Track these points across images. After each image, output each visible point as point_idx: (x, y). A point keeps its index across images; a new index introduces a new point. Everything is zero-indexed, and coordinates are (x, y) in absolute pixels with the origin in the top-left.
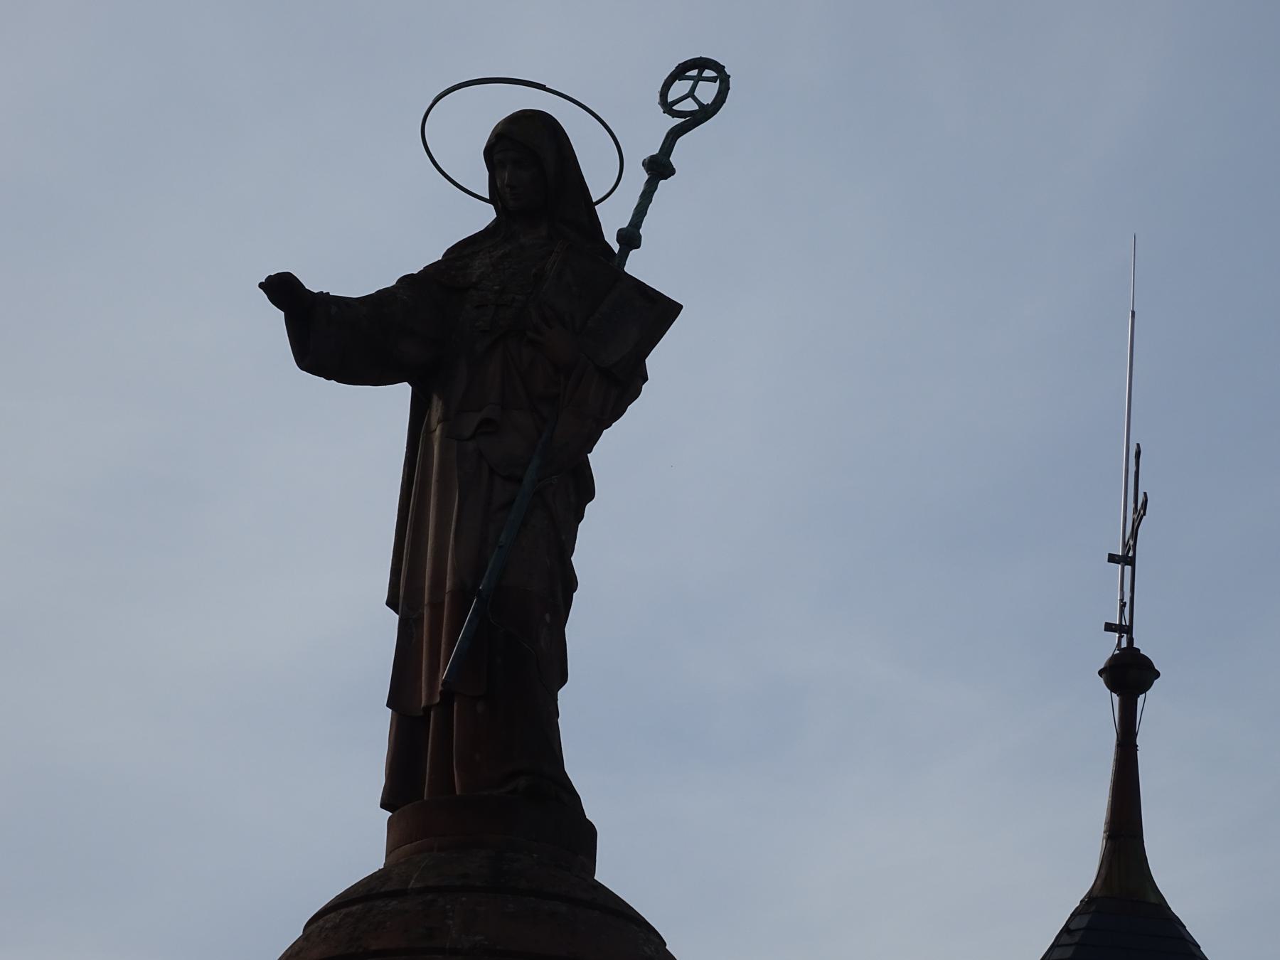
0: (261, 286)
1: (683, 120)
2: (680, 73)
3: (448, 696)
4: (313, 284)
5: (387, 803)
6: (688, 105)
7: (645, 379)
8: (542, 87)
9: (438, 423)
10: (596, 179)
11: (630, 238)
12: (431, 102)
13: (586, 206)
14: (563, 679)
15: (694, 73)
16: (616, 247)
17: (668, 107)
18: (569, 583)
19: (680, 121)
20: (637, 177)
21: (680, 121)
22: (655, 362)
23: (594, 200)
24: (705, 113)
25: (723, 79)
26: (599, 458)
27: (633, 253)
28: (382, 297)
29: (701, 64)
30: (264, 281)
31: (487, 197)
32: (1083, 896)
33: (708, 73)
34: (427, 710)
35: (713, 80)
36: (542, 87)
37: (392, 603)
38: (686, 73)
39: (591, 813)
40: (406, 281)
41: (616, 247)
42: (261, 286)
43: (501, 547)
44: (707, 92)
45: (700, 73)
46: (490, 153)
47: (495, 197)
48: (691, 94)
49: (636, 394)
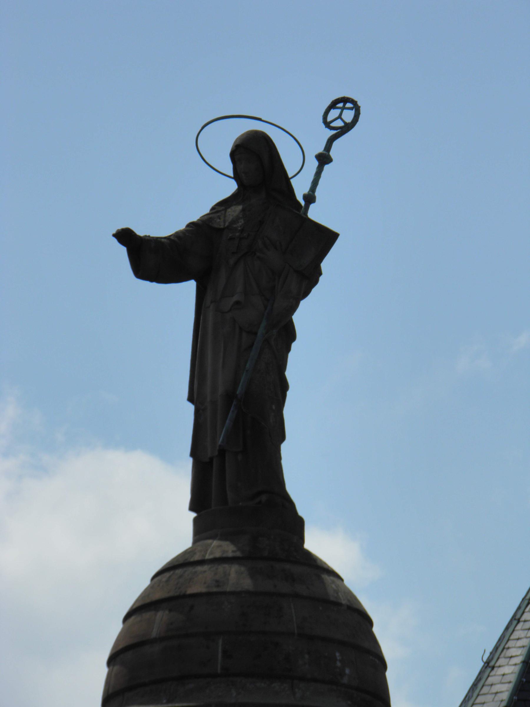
0: (114, 235)
1: (338, 131)
2: (333, 105)
3: (222, 452)
4: (140, 232)
5: (192, 508)
6: (339, 123)
7: (320, 274)
8: (260, 119)
9: (212, 302)
10: (290, 169)
11: (310, 198)
12: (200, 128)
13: (286, 180)
14: (282, 437)
15: (341, 105)
16: (303, 203)
17: (327, 124)
18: (284, 386)
19: (334, 132)
20: (312, 164)
21: (334, 132)
22: (325, 265)
23: (290, 175)
24: (347, 128)
25: (357, 108)
26: (297, 318)
27: (312, 206)
28: (179, 236)
29: (345, 100)
30: (193, 515)
31: (232, 175)
32: (163, 706)
33: (349, 105)
34: (211, 459)
35: (351, 109)
36: (260, 119)
37: (191, 399)
38: (336, 105)
39: (301, 511)
40: (192, 225)
41: (303, 203)
42: (114, 235)
43: (247, 371)
44: (348, 116)
45: (344, 105)
46: (233, 155)
47: (237, 177)
48: (340, 117)
49: (316, 282)
